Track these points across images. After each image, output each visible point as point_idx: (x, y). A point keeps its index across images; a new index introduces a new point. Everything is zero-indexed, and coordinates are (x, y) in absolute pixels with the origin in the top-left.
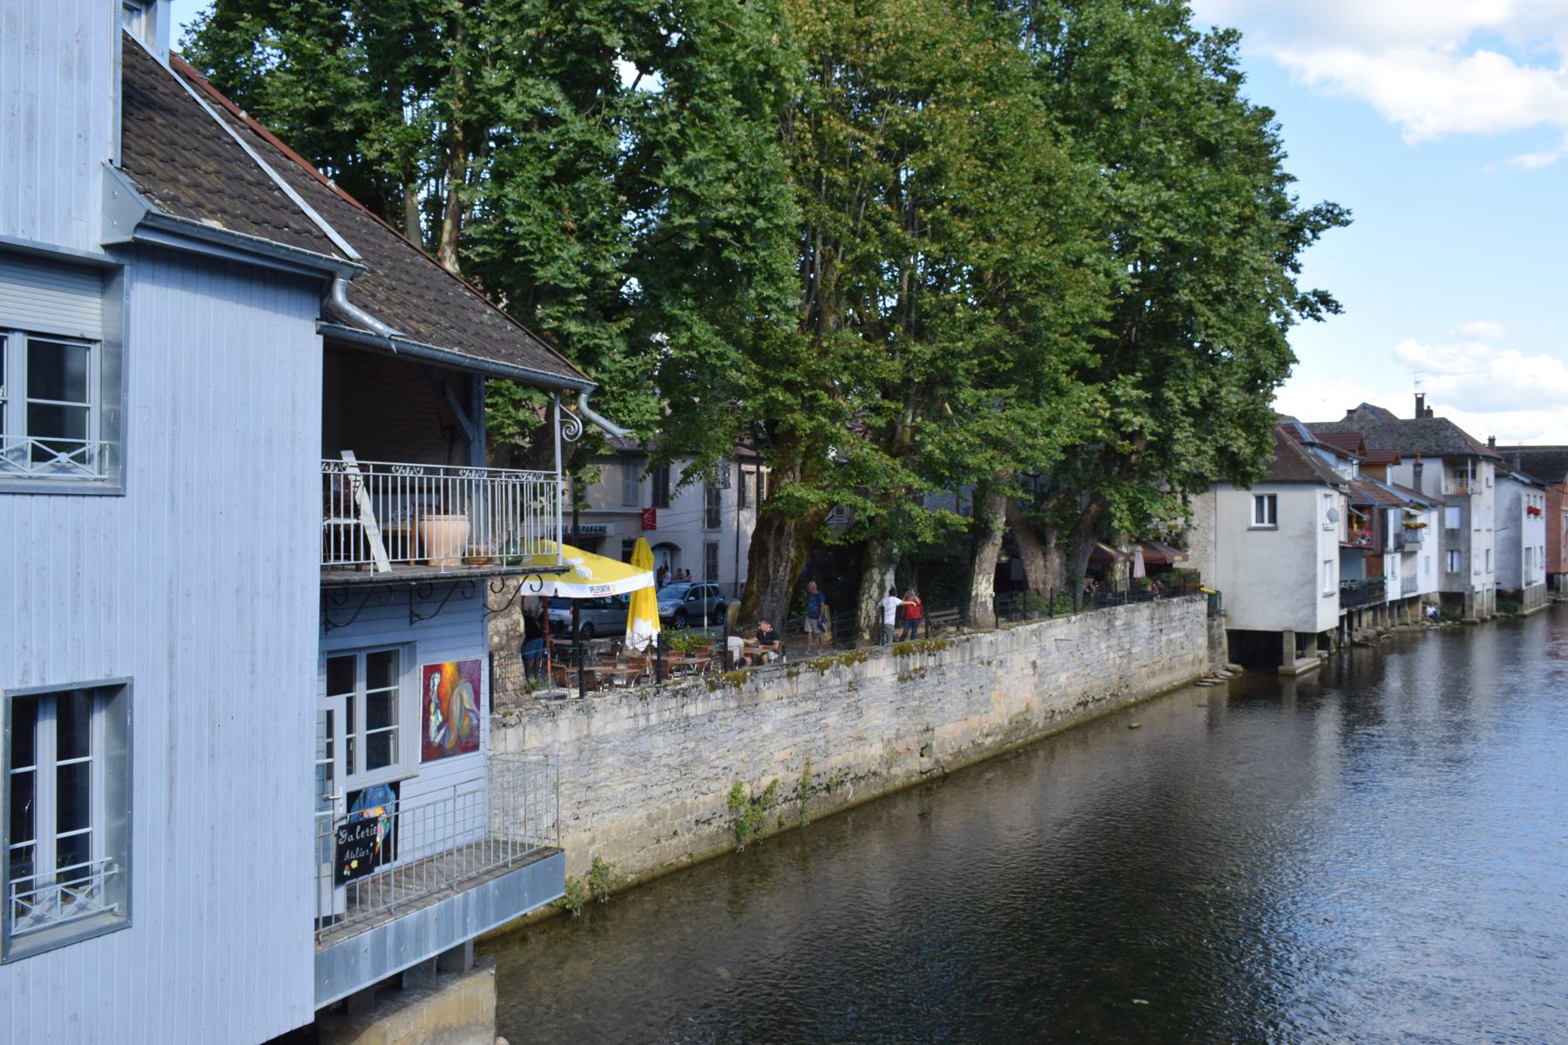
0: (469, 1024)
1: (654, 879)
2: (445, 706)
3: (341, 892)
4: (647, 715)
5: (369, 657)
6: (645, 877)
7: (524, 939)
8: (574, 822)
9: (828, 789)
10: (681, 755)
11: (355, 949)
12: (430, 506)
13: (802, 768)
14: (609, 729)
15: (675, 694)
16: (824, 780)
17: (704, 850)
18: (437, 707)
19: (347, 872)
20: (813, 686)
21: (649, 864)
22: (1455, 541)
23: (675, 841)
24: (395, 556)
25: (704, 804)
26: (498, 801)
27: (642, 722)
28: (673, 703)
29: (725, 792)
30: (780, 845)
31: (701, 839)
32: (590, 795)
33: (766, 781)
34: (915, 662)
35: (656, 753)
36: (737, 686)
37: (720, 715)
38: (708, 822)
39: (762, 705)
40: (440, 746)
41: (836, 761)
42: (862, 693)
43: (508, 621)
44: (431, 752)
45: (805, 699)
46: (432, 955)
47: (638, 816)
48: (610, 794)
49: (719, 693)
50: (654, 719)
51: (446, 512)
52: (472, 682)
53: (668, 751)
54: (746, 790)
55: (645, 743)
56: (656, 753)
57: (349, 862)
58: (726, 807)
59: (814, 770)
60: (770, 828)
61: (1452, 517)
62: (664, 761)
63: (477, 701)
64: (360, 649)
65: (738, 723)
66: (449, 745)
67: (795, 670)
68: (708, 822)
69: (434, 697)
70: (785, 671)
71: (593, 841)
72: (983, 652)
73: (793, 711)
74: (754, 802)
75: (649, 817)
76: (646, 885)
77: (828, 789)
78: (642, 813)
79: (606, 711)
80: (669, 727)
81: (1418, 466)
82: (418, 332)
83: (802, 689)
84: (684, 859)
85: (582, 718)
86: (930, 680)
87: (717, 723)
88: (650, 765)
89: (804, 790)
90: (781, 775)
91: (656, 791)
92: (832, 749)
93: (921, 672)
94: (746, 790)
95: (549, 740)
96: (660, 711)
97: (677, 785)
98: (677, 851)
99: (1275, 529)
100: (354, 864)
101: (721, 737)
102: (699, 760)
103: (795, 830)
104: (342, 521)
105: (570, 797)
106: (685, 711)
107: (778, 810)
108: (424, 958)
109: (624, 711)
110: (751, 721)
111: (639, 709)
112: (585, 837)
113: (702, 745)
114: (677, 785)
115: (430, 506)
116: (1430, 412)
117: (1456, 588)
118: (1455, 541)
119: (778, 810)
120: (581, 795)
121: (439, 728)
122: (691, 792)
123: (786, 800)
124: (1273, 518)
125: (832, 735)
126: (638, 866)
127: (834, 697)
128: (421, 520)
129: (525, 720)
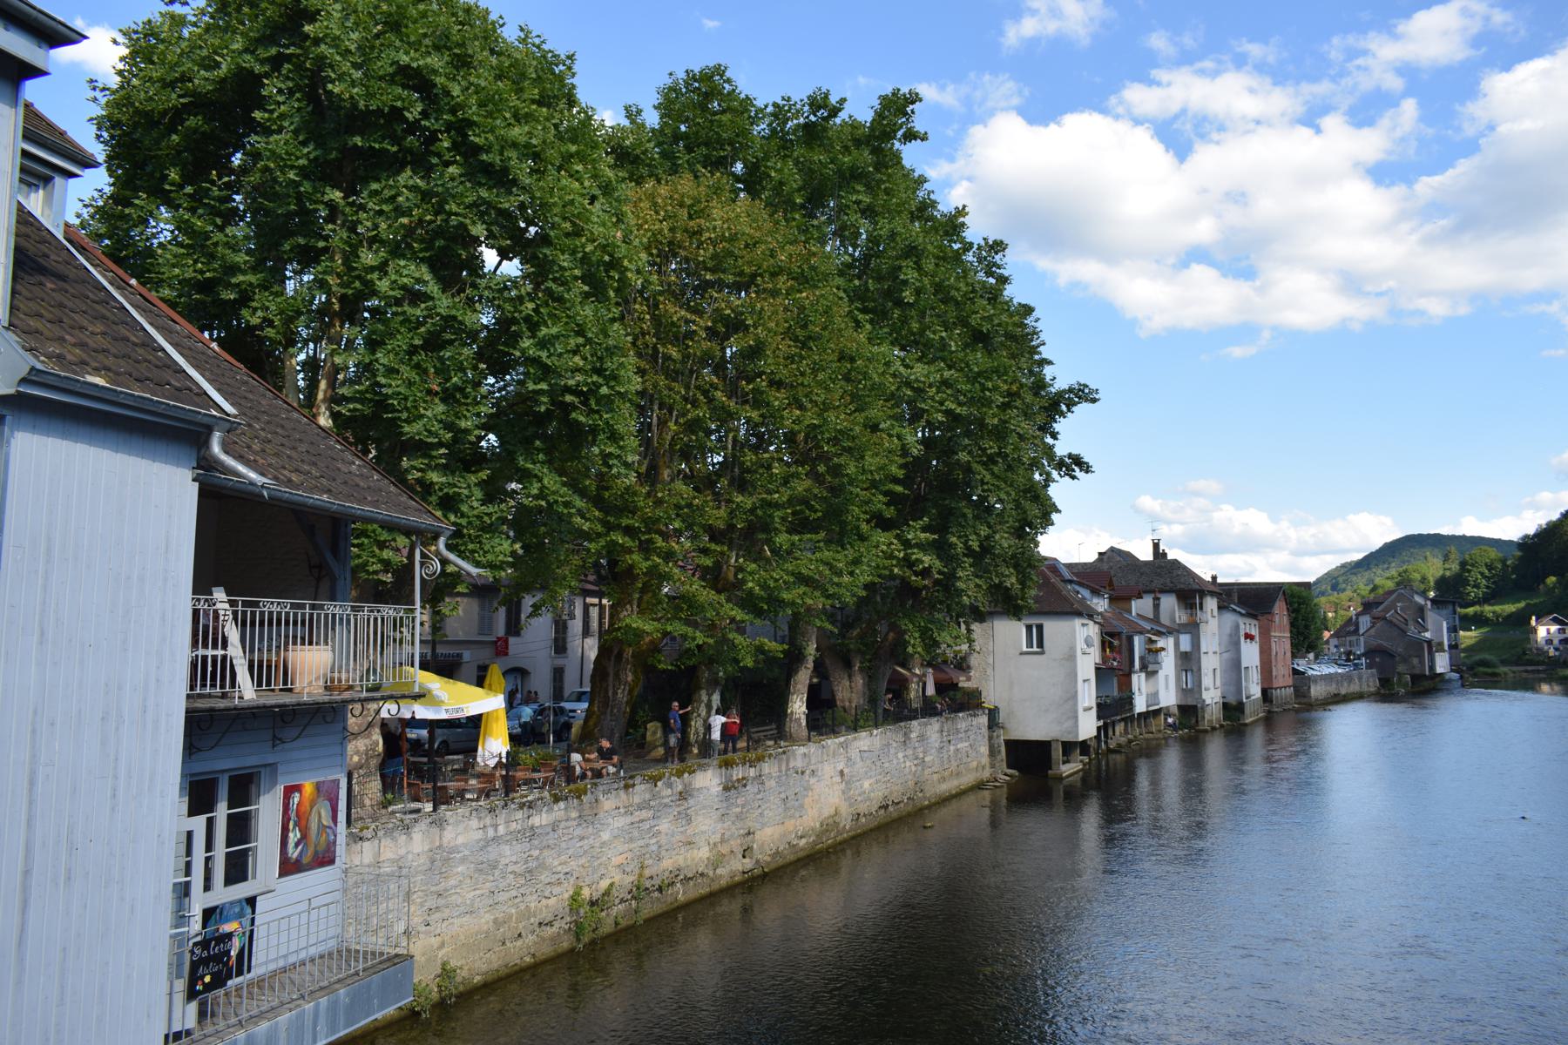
1: (500, 979)
4: (496, 826)
6: (490, 978)
9: (660, 889)
10: (526, 862)
12: (295, 637)
13: (637, 871)
14: (460, 840)
15: (522, 806)
16: (657, 882)
18: (296, 824)
19: (199, 987)
22: (1189, 662)
23: (519, 943)
27: (491, 833)
28: (519, 815)
29: (566, 896)
30: (617, 941)
31: (543, 939)
32: (441, 902)
33: (604, 884)
34: (738, 773)
35: (503, 861)
36: (579, 797)
37: (562, 825)
38: (550, 924)
40: (298, 861)
41: (667, 864)
42: (691, 802)
43: (367, 741)
44: (288, 867)
47: (485, 920)
49: (562, 804)
50: (501, 830)
55: (492, 852)
56: (503, 861)
59: (647, 873)
61: (1185, 642)
62: (510, 869)
63: (335, 819)
65: (579, 831)
66: (305, 860)
68: (550, 924)
69: (293, 815)
71: (442, 945)
72: (798, 763)
73: (629, 819)
75: (495, 921)
76: (493, 985)
77: (660, 889)
78: (489, 917)
79: (458, 823)
80: (516, 836)
81: (1156, 599)
82: (290, 481)
83: (637, 800)
84: (528, 959)
85: (435, 830)
86: (752, 788)
88: (497, 873)
89: (638, 892)
90: (618, 878)
92: (663, 853)
93: (743, 782)
94: (586, 893)
95: (402, 852)
97: (522, 891)
98: (520, 952)
99: (1042, 653)
101: (564, 845)
102: (542, 866)
103: (630, 929)
104: (210, 652)
109: (474, 823)
111: (488, 821)
112: (435, 941)
113: (546, 853)
114: (522, 891)
115: (295, 637)
116: (1165, 554)
117: (1190, 702)
118: (1189, 662)
120: (431, 903)
121: (297, 845)
123: (622, 901)
124: (1041, 644)
126: (484, 968)
127: (666, 805)
128: (286, 650)
129: (381, 833)
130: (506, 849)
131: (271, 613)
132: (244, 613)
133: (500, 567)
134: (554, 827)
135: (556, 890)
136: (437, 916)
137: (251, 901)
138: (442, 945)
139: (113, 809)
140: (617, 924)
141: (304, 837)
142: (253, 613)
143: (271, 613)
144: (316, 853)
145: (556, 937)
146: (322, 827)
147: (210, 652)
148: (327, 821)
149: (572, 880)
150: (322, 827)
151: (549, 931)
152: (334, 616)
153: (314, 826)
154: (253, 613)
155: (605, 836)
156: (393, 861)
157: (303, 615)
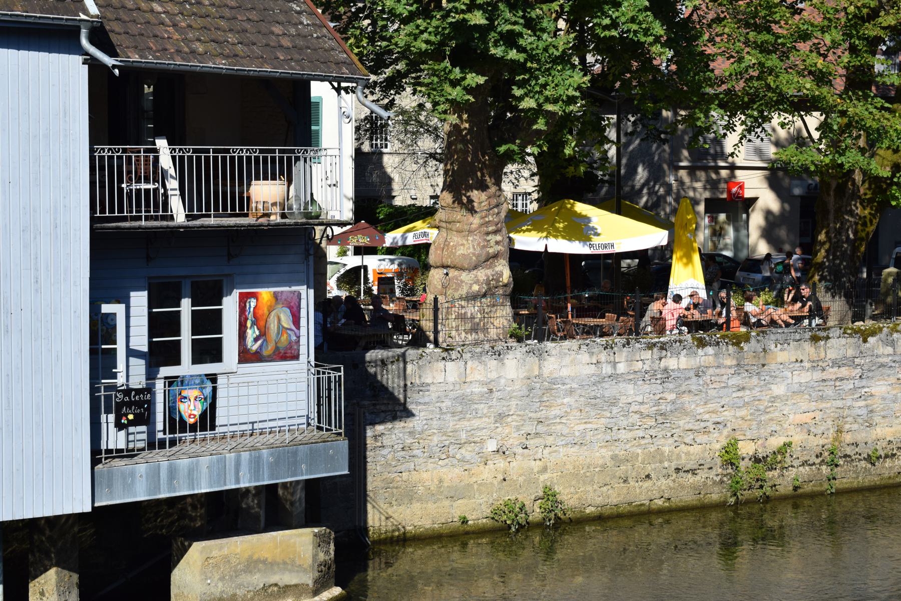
0: (285, 563)
1: (620, 516)
2: (262, 323)
3: (122, 433)
4: (615, 364)
5: (193, 283)
6: (607, 511)
7: (464, 545)
8: (520, 450)
9: (869, 459)
10: (657, 403)
11: (132, 474)
12: (129, 172)
13: (831, 433)
14: (565, 372)
15: (651, 346)
16: (865, 451)
17: (687, 497)
18: (253, 324)
19: (124, 421)
20: (850, 352)
21: (614, 500)
23: (647, 484)
24: (191, 209)
25: (688, 454)
26: (435, 423)
27: (607, 369)
28: (647, 355)
29: (718, 446)
30: (796, 506)
31: (682, 487)
32: (541, 429)
33: (776, 442)
35: (623, 400)
36: (737, 344)
37: (711, 371)
38: (693, 472)
39: (773, 366)
40: (257, 352)
43: (489, 272)
44: (246, 356)
45: (836, 364)
46: (204, 491)
47: (602, 454)
48: (566, 431)
49: (710, 350)
50: (622, 368)
51: (265, 178)
52: (290, 308)
53: (640, 399)
54: (746, 449)
55: (610, 389)
56: (623, 400)
57: (126, 415)
58: (719, 461)
59: (848, 438)
60: (785, 487)
62: (634, 408)
63: (296, 321)
64: (185, 277)
65: (735, 381)
66: (266, 353)
67: (822, 334)
68: (693, 472)
69: (250, 316)
70: (808, 335)
71: (545, 469)
73: (817, 375)
74: (757, 460)
75: (614, 457)
76: (604, 519)
77: (869, 459)
78: (606, 453)
79: (562, 355)
80: (647, 376)
82: (193, 52)
83: (832, 354)
84: (660, 502)
85: (532, 360)
87: (707, 378)
88: (615, 410)
89: (832, 458)
90: (798, 438)
91: (624, 435)
92: (877, 419)
94: (746, 449)
95: (493, 375)
96: (630, 361)
97: (653, 432)
98: (643, 494)
100: (131, 417)
101: (712, 393)
102: (682, 411)
103: (822, 494)
104: (143, 186)
105: (518, 428)
106: (663, 363)
107: (792, 473)
108: (196, 492)
109: (584, 357)
110: (755, 380)
111: (603, 356)
112: (536, 466)
113: (686, 398)
114: (653, 432)
115: (129, 172)
119: (792, 473)
120: (530, 428)
121: (256, 340)
122: (671, 441)
123: (805, 463)
125: (877, 404)
126: (599, 501)
127: (882, 365)
128: (249, 185)
129: (467, 356)
130: (630, 389)
131: (240, 158)
132: (281, 159)
133: (571, 100)
134: (698, 373)
135: (701, 438)
136: (537, 441)
137: (213, 378)
138: (545, 469)
139: (37, 290)
140: (796, 488)
141: (263, 334)
142: (224, 158)
143: (240, 158)
144: (277, 348)
145: (710, 484)
146: (281, 329)
147: (143, 186)
148: (287, 322)
149: (725, 432)
150: (281, 329)
151: (690, 479)
152: (241, 158)
153: (273, 327)
154: (224, 158)
155: (779, 389)
156: (483, 384)
157: (207, 159)
